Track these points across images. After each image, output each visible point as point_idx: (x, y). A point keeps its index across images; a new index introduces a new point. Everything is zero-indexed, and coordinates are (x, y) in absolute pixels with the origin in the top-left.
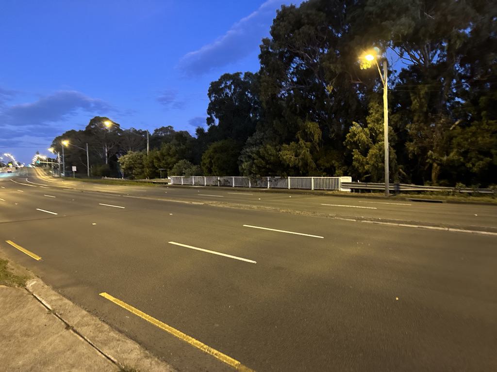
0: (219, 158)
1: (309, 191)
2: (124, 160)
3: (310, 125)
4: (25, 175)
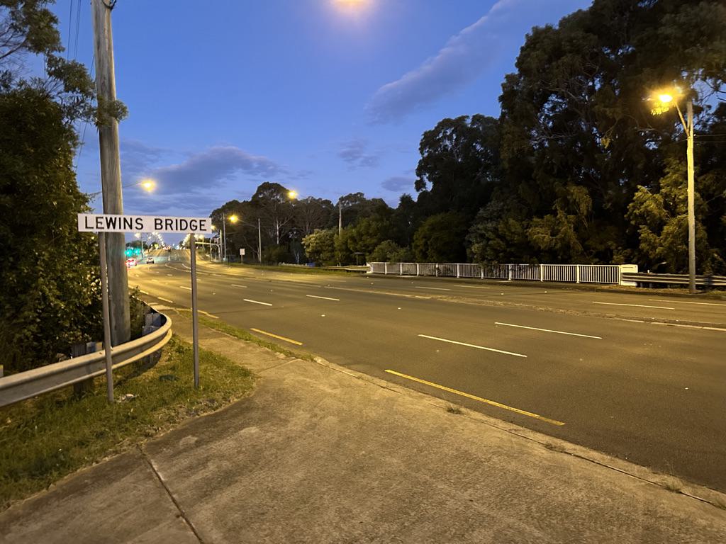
0: (437, 238)
1: (574, 284)
2: (311, 240)
3: (574, 189)
4: (178, 259)
